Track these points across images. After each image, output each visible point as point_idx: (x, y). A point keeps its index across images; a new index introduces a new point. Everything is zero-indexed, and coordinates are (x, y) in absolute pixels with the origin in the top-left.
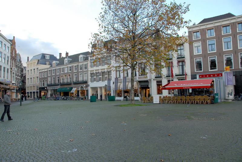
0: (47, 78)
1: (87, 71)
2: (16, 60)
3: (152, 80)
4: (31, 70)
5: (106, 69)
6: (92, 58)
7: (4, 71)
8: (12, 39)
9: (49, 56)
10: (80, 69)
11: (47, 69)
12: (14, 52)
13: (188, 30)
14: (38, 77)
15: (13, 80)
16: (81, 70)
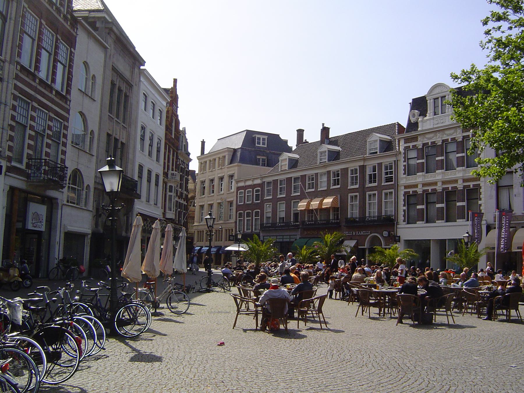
0: (261, 206)
1: (396, 187)
2: (178, 150)
4: (212, 181)
6: (411, 145)
7: (149, 181)
9: (266, 137)
12: (174, 124)
14: (231, 203)
16: (375, 182)
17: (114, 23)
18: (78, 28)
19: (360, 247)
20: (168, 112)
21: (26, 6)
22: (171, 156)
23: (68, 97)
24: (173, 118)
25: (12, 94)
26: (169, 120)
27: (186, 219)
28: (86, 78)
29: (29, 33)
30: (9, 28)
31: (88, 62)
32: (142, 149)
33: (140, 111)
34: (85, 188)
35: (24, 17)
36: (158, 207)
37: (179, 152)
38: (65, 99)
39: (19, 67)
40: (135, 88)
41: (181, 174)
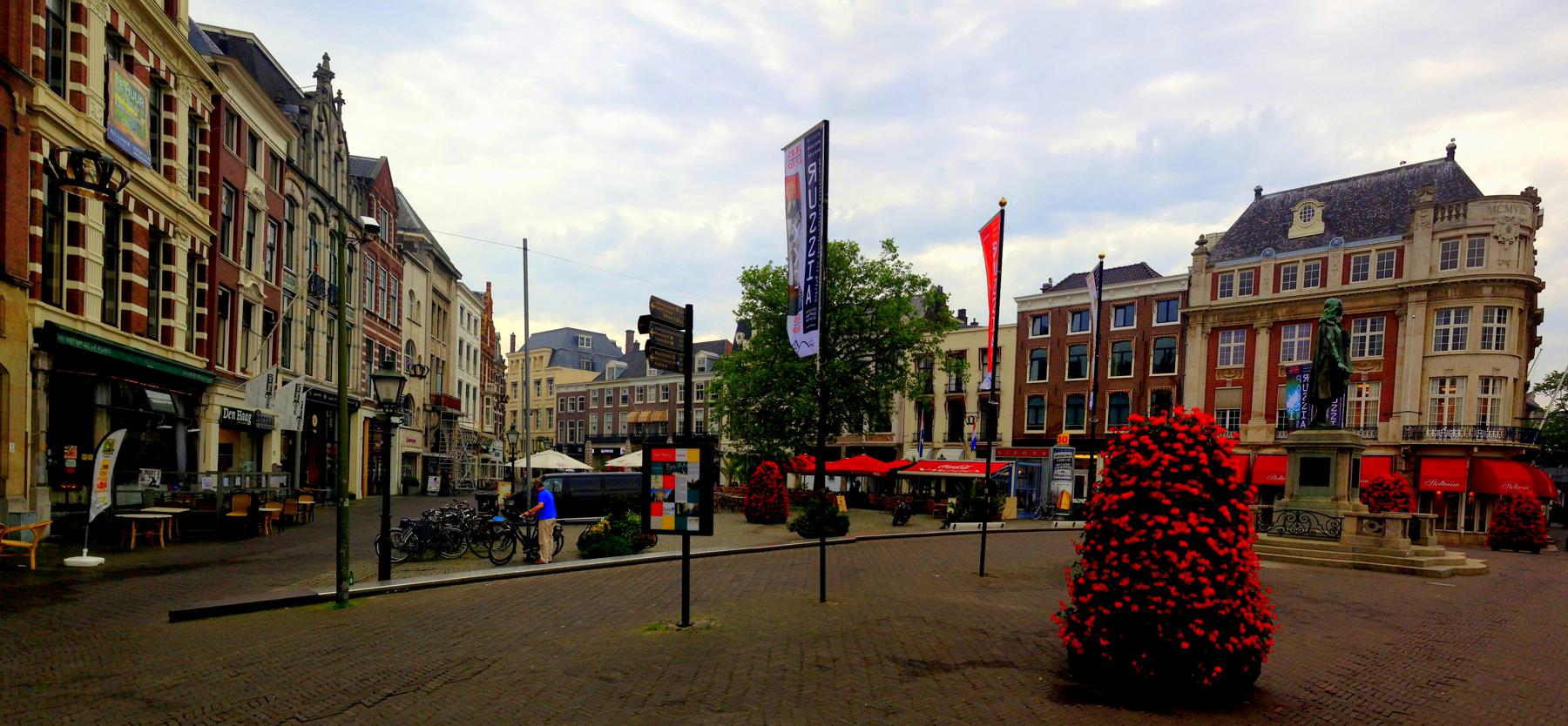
8: (483, 290)
11: (588, 385)
13: (1019, 307)
14: (550, 410)
15: (488, 423)
17: (434, 243)
38: (397, 330)
40: (452, 303)
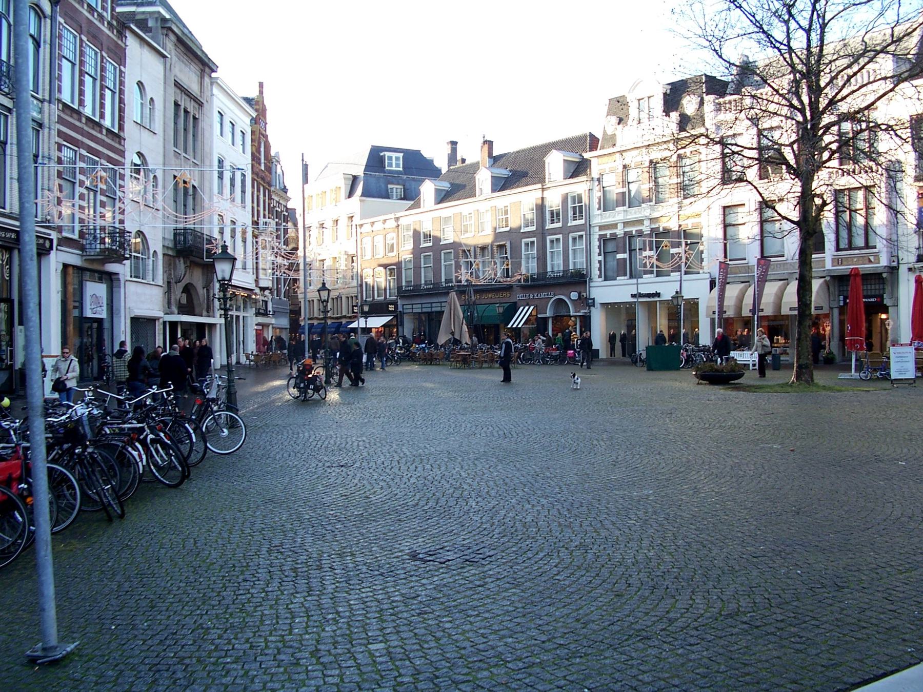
1: (587, 227)
2: (270, 185)
3: (903, 269)
5: (620, 226)
8: (253, 93)
9: (401, 155)
10: (575, 213)
12: (262, 149)
18: (127, 35)
19: (539, 316)
20: (253, 133)
21: (62, 21)
22: (262, 196)
23: (122, 134)
24: (261, 140)
25: (56, 143)
26: (256, 144)
27: (288, 285)
28: (142, 104)
29: (68, 57)
30: (44, 56)
31: (142, 81)
32: (221, 192)
33: (215, 138)
34: (151, 255)
35: (60, 37)
36: (248, 273)
37: (273, 189)
38: (118, 137)
39: (61, 106)
41: (277, 220)
